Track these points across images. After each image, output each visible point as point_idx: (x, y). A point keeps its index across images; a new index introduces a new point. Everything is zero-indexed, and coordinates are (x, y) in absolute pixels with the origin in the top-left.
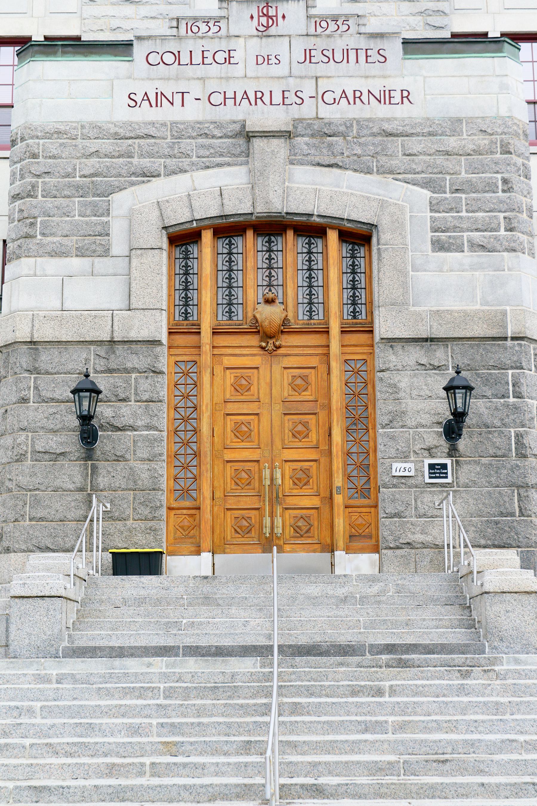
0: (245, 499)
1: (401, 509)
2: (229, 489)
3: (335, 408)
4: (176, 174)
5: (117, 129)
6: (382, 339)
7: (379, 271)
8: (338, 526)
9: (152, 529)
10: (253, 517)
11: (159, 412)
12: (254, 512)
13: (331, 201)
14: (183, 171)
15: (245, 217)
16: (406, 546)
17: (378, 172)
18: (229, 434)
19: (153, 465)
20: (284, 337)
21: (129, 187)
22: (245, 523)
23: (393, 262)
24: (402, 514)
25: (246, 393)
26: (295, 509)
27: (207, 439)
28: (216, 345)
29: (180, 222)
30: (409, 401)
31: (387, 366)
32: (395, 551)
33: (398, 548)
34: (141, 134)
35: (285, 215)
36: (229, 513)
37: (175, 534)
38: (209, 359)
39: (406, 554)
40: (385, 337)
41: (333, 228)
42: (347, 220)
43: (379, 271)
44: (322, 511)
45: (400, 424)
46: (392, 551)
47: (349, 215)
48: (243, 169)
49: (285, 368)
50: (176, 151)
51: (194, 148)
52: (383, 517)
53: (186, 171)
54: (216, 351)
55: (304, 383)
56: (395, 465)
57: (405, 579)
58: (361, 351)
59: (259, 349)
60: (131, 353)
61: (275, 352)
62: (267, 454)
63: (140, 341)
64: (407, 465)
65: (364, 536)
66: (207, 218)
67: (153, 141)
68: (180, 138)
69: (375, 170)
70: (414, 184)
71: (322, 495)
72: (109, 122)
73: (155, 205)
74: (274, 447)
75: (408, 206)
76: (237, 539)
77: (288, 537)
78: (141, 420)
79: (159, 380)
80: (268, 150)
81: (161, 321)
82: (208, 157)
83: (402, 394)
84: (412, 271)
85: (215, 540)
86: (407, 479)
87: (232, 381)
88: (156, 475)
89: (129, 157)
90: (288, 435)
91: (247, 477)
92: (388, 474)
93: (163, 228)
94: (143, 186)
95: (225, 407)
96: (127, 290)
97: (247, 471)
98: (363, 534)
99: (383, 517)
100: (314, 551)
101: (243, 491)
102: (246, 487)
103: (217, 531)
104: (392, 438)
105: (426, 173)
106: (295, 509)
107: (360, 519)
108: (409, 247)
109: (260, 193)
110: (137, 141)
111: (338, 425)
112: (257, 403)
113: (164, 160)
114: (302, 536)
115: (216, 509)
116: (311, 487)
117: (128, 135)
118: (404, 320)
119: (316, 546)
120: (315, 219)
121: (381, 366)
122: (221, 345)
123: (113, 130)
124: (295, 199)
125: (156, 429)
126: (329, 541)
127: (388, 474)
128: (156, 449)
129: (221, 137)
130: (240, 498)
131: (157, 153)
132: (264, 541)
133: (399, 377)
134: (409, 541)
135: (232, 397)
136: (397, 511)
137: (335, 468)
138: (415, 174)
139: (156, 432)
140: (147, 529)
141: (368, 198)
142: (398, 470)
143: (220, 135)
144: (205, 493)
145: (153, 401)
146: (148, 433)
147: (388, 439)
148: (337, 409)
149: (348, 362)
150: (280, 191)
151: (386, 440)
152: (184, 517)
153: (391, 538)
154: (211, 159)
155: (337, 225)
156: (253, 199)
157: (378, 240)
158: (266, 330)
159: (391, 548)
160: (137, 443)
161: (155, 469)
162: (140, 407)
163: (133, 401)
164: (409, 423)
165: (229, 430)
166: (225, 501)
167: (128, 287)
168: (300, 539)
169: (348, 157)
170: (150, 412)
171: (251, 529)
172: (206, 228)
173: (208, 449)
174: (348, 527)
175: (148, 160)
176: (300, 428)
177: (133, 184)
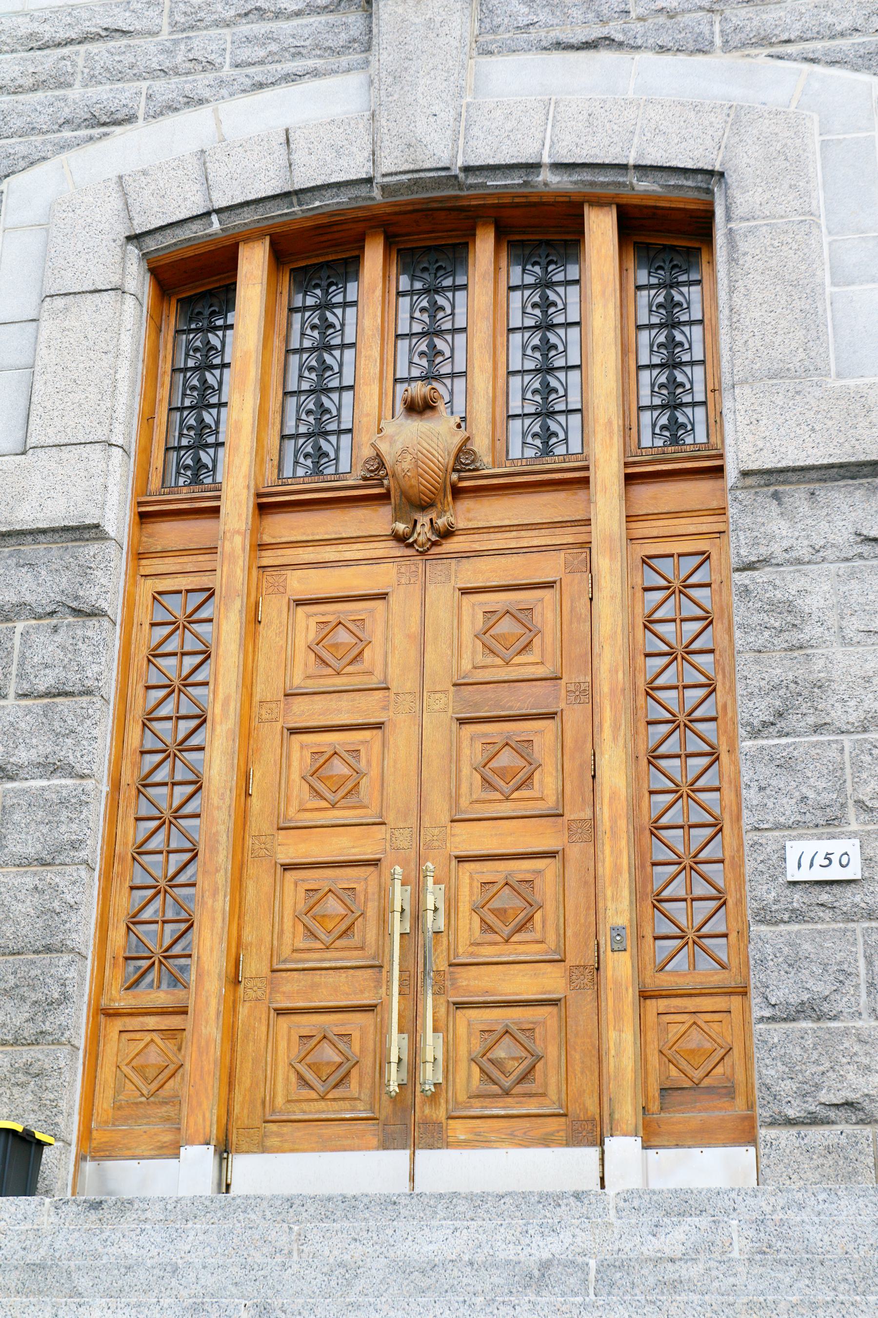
0: (331, 978)
1: (822, 988)
2: (286, 951)
3: (606, 689)
4: (176, 109)
5: (35, 27)
6: (745, 474)
7: (732, 290)
8: (617, 1055)
9: (33, 1070)
10: (356, 1035)
11: (81, 723)
12: (358, 1017)
13: (590, 125)
14: (194, 102)
15: (353, 192)
16: (842, 1113)
17: (727, 46)
18: (299, 790)
19: (51, 875)
20: (466, 505)
21: (55, 153)
22: (329, 1054)
23: (774, 262)
24: (826, 1007)
25: (350, 669)
26: (486, 1005)
27: (222, 797)
28: (267, 539)
29: (174, 219)
30: (838, 652)
31: (763, 551)
32: (804, 1130)
33: (814, 1120)
34: (93, 30)
35: (462, 175)
36: (284, 1022)
37: (118, 1091)
38: (239, 572)
39: (843, 1140)
40: (754, 466)
41: (599, 202)
42: (637, 167)
43: (732, 290)
44: (572, 1011)
45: (811, 720)
46: (793, 1131)
47: (642, 155)
48: (356, 79)
49: (465, 591)
50: (180, 58)
51: (229, 46)
52: (762, 1019)
53: (201, 102)
54: (269, 557)
55: (519, 630)
56: (795, 849)
57: (801, 1207)
58: (692, 529)
59: (392, 544)
60: (18, 565)
61: (435, 550)
62: (403, 840)
63: (43, 531)
64: (836, 847)
65: (709, 1089)
66: (247, 203)
67: (124, 42)
68: (192, 28)
69: (718, 41)
70: (833, 63)
71: (572, 959)
72: (17, 14)
73: (113, 185)
74: (426, 819)
75: (816, 117)
76: (304, 1105)
77: (462, 1097)
78: (29, 747)
79: (89, 633)
80: (417, 20)
81: (106, 473)
82: (262, 62)
83: (811, 631)
84: (834, 284)
85: (237, 1109)
86: (836, 889)
87: (312, 635)
88: (56, 905)
89: (61, 85)
90: (471, 780)
91: (341, 910)
92: (774, 878)
93: (129, 239)
94: (91, 149)
95: (287, 710)
96: (23, 402)
97: (344, 896)
98: (706, 1082)
99: (762, 1019)
100: (546, 1142)
101: (328, 955)
102: (339, 943)
103: (244, 1080)
104: (786, 765)
105: (865, 33)
106: (486, 1005)
107: (695, 1032)
108: (823, 221)
109: (391, 125)
110: (82, 48)
111: (615, 738)
112: (380, 694)
113: (147, 83)
114: (507, 1093)
115: (243, 1011)
116: (538, 936)
117: (62, 35)
118: (810, 415)
119: (553, 1124)
120: (546, 176)
121: (744, 552)
122: (284, 540)
123: (25, 27)
124: (489, 131)
125: (70, 772)
126: (592, 1107)
127: (774, 878)
128: (63, 828)
129: (298, 14)
130: (317, 977)
131: (131, 67)
132: (386, 1110)
133: (802, 583)
134: (852, 1096)
135: (310, 682)
136: (805, 997)
137: (606, 869)
138: (833, 37)
139: (69, 782)
140: (18, 1070)
141: (696, 108)
142: (806, 862)
143: (295, 8)
144: (204, 958)
145: (66, 694)
146: (44, 783)
147: (772, 769)
148: (612, 691)
149: (651, 562)
150: (447, 116)
151: (765, 771)
152: (148, 1037)
153: (788, 1086)
154: (269, 67)
155: (612, 190)
156: (374, 143)
157: (728, 209)
158: (405, 484)
159: (790, 1122)
160: (11, 813)
161: (55, 888)
162: (30, 711)
163: (12, 695)
164: (837, 715)
165: (295, 776)
166: (273, 987)
167: (26, 395)
168: (501, 1102)
169: (641, 19)
170: (56, 724)
171: (348, 1074)
172: (251, 236)
173: (222, 828)
174: (654, 1059)
175: (108, 87)
176: (506, 759)
177: (64, 147)
